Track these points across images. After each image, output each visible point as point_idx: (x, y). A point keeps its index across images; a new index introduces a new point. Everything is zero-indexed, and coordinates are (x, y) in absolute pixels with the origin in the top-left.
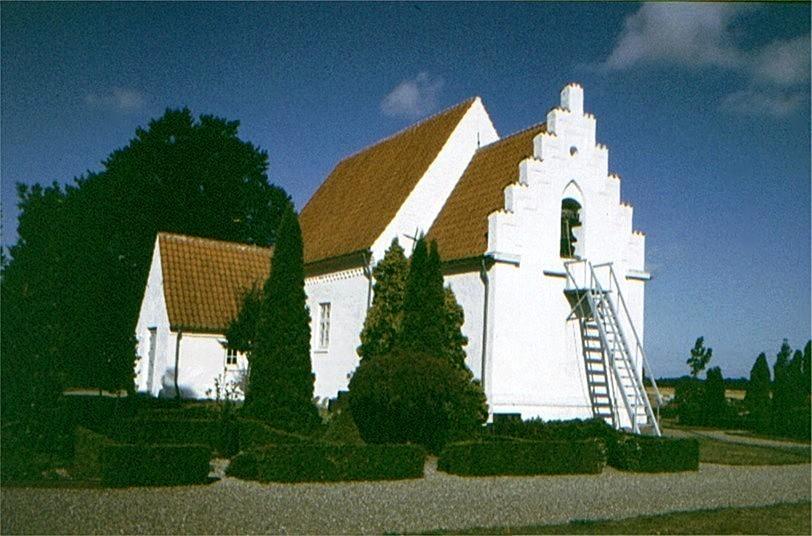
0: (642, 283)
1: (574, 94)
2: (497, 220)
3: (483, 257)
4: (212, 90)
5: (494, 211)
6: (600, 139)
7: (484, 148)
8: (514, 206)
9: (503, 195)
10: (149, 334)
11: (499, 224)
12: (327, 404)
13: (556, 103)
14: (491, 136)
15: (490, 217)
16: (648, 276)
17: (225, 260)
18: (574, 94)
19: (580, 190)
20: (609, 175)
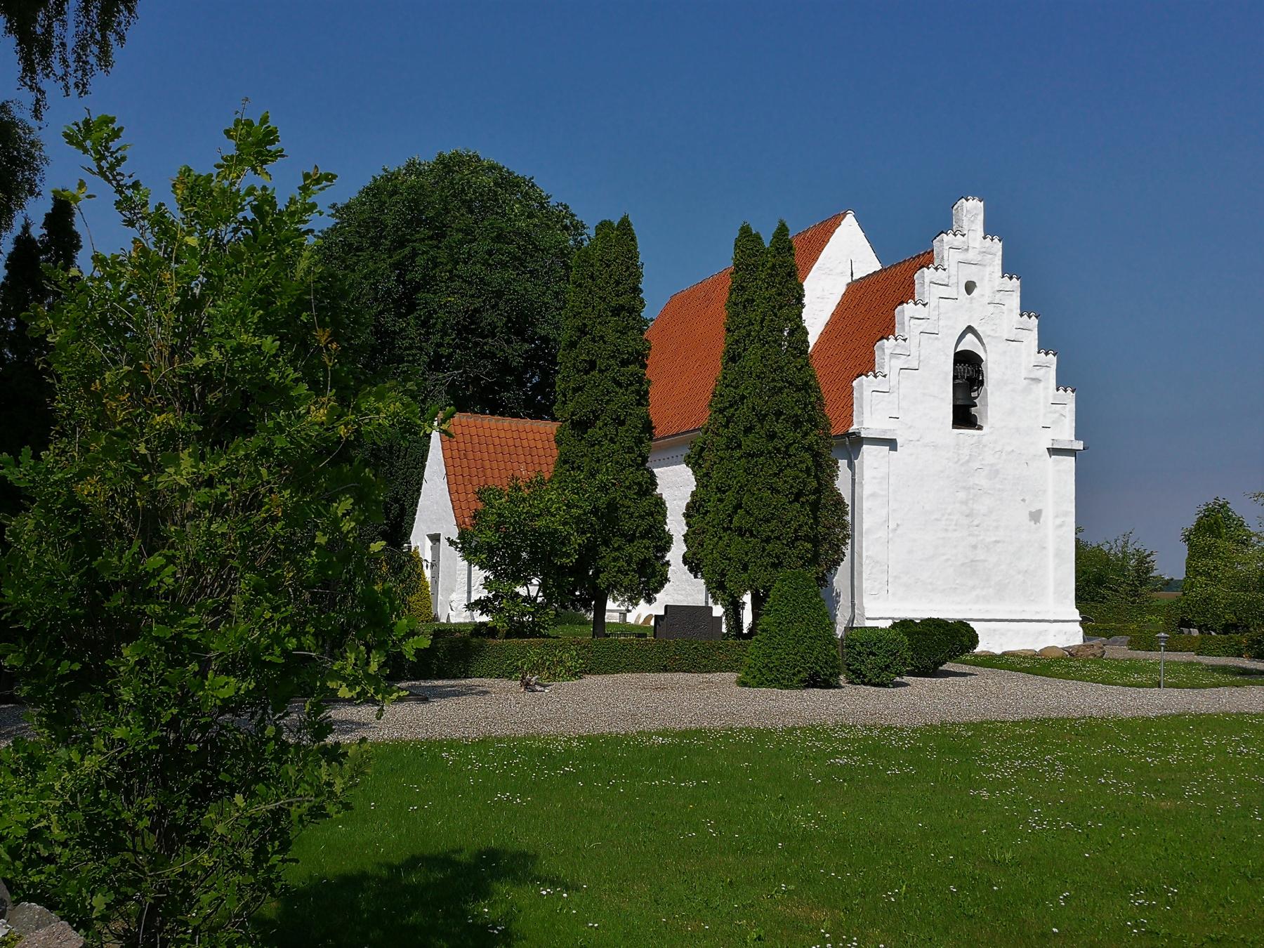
0: (1070, 461)
1: (971, 211)
2: (864, 386)
3: (848, 435)
4: (281, 278)
5: (859, 376)
6: (1009, 269)
7: (857, 281)
8: (926, 294)
9: (873, 353)
10: (429, 543)
11: (867, 393)
12: (652, 623)
13: (945, 224)
14: (869, 264)
15: (854, 383)
16: (1079, 445)
17: (525, 443)
18: (971, 211)
19: (983, 344)
20: (1021, 315)
